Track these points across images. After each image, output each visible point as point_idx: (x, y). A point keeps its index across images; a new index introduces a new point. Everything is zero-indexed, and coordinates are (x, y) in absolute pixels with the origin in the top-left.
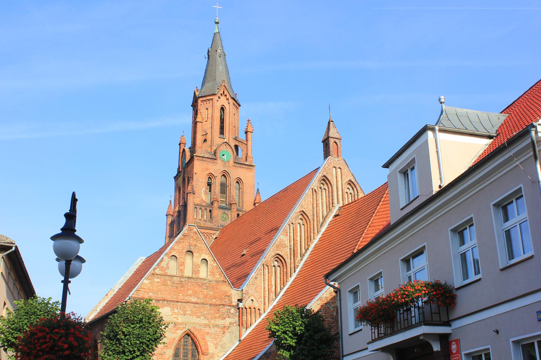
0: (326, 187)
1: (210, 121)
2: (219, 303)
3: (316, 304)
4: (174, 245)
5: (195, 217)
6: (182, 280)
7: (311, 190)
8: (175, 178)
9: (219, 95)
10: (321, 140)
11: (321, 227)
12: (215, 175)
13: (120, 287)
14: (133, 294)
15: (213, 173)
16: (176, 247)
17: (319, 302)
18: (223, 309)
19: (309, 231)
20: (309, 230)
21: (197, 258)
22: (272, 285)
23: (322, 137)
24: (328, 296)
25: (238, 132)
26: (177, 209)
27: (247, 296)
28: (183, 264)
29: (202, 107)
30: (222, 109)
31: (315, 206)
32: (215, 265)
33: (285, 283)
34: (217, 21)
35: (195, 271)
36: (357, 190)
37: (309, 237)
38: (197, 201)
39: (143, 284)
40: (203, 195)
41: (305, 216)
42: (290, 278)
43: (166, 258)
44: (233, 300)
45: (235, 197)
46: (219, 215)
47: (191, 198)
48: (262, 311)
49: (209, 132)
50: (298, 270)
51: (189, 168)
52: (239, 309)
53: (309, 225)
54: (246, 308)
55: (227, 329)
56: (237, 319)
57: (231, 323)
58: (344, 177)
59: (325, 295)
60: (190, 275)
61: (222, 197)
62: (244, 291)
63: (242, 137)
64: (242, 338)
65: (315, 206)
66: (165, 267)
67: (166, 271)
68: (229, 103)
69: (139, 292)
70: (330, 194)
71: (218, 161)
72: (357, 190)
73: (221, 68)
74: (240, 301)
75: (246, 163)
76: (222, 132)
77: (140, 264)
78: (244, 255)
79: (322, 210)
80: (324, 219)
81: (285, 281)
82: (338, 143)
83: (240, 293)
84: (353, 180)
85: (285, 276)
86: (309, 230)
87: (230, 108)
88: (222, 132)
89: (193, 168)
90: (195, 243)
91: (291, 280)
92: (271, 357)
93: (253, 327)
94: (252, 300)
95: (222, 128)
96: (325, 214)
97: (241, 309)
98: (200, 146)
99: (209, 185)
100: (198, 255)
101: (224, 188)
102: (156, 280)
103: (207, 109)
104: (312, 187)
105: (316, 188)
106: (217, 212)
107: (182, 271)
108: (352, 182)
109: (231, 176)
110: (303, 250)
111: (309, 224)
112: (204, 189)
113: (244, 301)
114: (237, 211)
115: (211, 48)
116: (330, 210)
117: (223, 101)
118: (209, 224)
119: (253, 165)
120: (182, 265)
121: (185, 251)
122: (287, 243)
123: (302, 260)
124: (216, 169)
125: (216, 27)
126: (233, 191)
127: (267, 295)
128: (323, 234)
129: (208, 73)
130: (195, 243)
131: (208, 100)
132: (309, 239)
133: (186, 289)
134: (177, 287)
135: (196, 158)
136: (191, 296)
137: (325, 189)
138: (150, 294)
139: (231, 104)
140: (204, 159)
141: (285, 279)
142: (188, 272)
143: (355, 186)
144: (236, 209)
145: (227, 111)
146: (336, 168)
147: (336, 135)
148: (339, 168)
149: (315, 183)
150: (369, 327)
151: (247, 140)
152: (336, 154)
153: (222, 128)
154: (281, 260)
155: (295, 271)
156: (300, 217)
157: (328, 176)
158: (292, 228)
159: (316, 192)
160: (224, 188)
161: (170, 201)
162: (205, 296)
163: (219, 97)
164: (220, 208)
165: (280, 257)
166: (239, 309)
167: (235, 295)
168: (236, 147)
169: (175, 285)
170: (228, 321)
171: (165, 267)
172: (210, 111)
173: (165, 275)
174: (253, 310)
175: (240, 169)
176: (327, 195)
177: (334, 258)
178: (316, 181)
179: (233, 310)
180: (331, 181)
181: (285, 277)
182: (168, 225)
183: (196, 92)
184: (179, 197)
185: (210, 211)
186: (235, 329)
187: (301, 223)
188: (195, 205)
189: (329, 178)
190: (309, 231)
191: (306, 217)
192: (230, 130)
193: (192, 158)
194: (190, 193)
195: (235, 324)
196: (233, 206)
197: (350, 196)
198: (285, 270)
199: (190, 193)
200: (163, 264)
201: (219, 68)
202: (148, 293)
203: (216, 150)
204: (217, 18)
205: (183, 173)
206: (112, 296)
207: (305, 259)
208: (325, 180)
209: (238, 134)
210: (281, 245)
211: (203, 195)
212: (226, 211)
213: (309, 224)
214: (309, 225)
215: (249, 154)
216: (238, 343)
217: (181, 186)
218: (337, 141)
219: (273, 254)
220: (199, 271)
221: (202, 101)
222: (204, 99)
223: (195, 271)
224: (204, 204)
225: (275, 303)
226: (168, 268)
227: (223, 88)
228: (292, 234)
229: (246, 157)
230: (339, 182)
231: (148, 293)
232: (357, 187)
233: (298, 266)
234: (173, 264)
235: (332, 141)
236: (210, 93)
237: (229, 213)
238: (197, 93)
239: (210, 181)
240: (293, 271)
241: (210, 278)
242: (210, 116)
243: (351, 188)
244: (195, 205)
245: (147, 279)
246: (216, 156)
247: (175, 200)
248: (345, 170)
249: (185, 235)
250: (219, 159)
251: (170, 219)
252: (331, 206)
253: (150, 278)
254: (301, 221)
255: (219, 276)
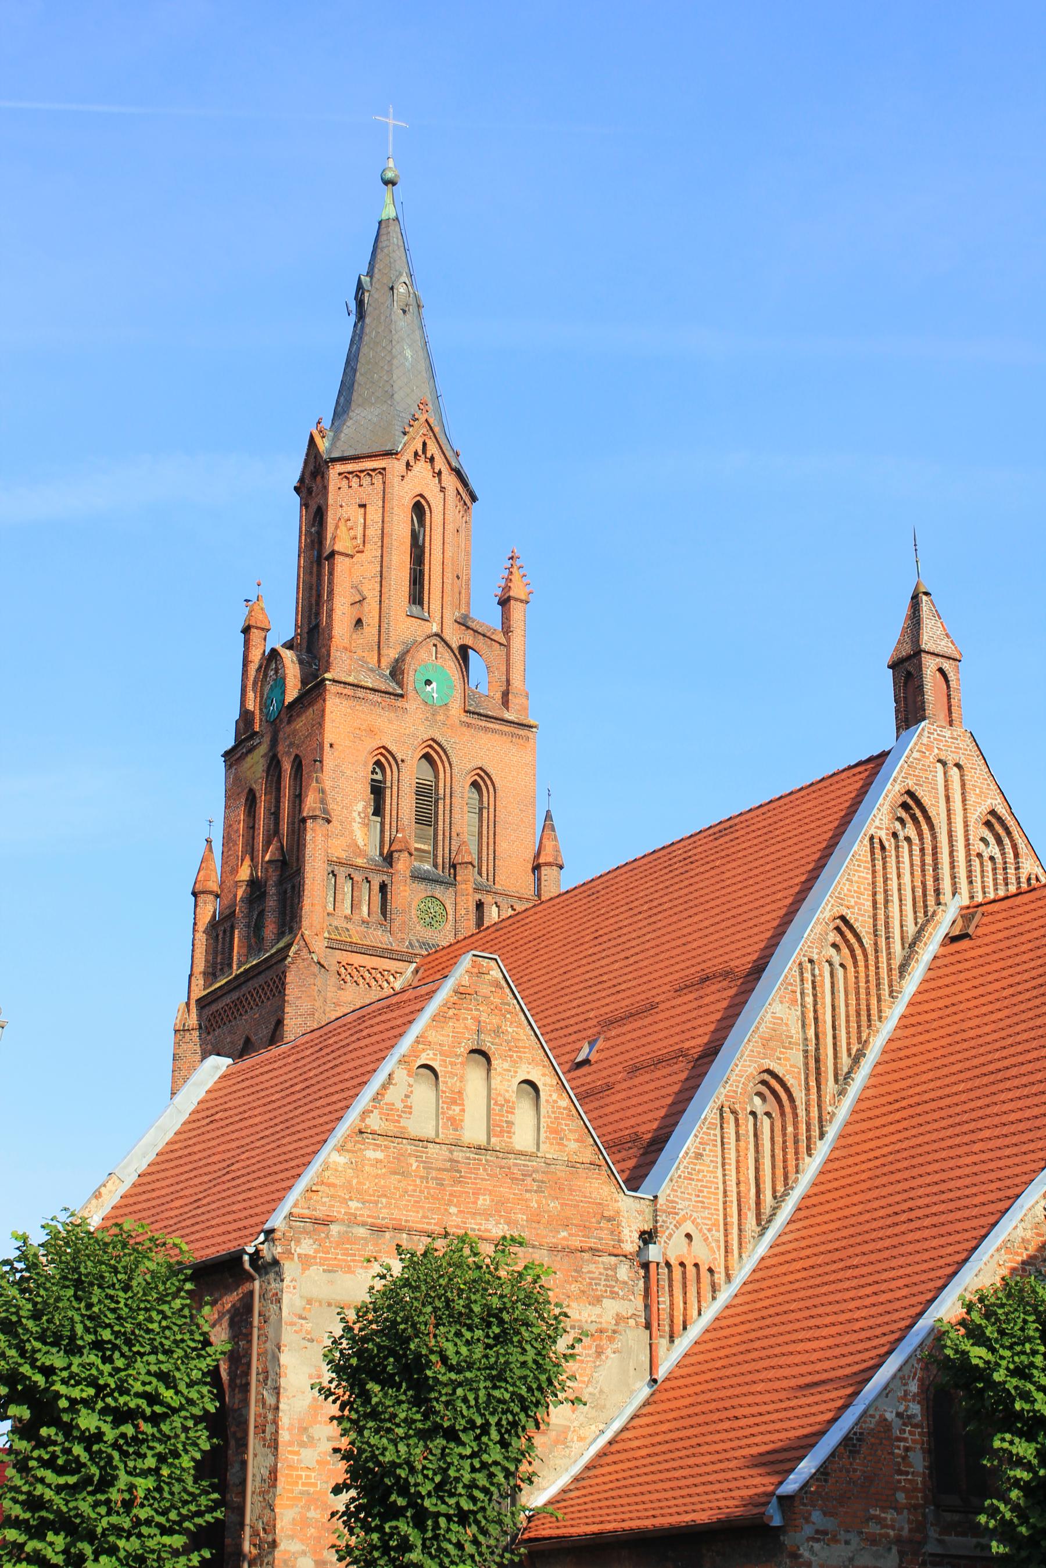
0: (911, 831)
1: (372, 551)
2: (578, 1245)
3: (993, 1263)
4: (428, 1027)
5: (330, 908)
6: (458, 1155)
7: (866, 842)
8: (227, 754)
9: (409, 456)
10: (887, 657)
11: (901, 976)
12: (399, 757)
13: (143, 1166)
14: (295, 1205)
15: (393, 748)
16: (432, 1036)
17: (1003, 1256)
18: (592, 1267)
19: (862, 991)
20: (862, 984)
21: (507, 1077)
22: (748, 1183)
23: (888, 643)
24: (1029, 1234)
25: (468, 595)
26: (244, 873)
27: (671, 1222)
28: (457, 1098)
29: (342, 497)
30: (419, 509)
31: (880, 898)
32: (564, 1103)
33: (792, 1176)
34: (389, 175)
35: (497, 1122)
36: (1015, 847)
37: (864, 1013)
38: (339, 852)
39: (326, 1167)
40: (356, 826)
41: (849, 936)
42: (807, 1159)
43: (401, 1075)
44: (626, 1231)
45: (466, 837)
46: (414, 905)
47: (320, 839)
48: (720, 1277)
49: (371, 591)
50: (832, 1131)
51: (300, 724)
52: (646, 1266)
53: (862, 969)
54: (668, 1265)
55: (611, 1339)
56: (640, 1303)
57: (619, 1319)
58: (971, 799)
59: (1020, 1232)
60: (482, 1140)
61: (420, 838)
62: (661, 1201)
63: (488, 616)
64: (661, 1373)
65: (880, 898)
66: (399, 1105)
67: (403, 1122)
68: (443, 489)
69: (314, 1196)
70: (929, 859)
71: (412, 704)
72: (1015, 847)
73: (408, 353)
74: (647, 1237)
75: (507, 716)
76: (417, 596)
77: (209, 1085)
78: (586, 1062)
79: (902, 917)
80: (912, 946)
81: (791, 1169)
82: (951, 676)
83: (648, 1212)
84: (1001, 811)
85: (791, 1150)
86: (862, 984)
87: (443, 508)
88: (417, 596)
89: (321, 725)
90: (495, 1020)
91: (812, 1167)
92: (863, 1450)
93: (695, 1331)
94: (688, 1236)
95: (417, 580)
96: (911, 929)
97: (653, 1267)
98: (345, 642)
99: (378, 791)
100: (506, 1065)
101: (428, 800)
102: (371, 1154)
103: (363, 506)
104: (872, 831)
105: (883, 834)
106: (407, 895)
107: (456, 1123)
108: (999, 819)
109: (453, 760)
110: (845, 1061)
111: (861, 963)
112: (360, 806)
113: (662, 1238)
114: (477, 890)
115: (370, 273)
116: (929, 918)
117: (422, 479)
118: (378, 937)
119: (532, 722)
120: (454, 1102)
121: (462, 1050)
122: (795, 1030)
123: (842, 1093)
124: (404, 731)
125: (388, 199)
126: (462, 817)
127: (735, 1219)
128: (910, 1004)
129: (361, 368)
130: (495, 1020)
131: (369, 472)
132: (865, 1018)
133: (469, 1189)
134: (440, 1184)
135: (331, 688)
136: (486, 1215)
137: (908, 839)
138: (354, 1205)
139: (451, 492)
140: (360, 693)
141: (791, 1163)
142: (474, 1131)
143: (1009, 833)
144: (471, 886)
145: (435, 517)
146: (944, 764)
147: (943, 646)
148: (958, 766)
149: (879, 816)
150: (363, 1297)
151: (507, 630)
152: (943, 714)
153: (417, 580)
154: (774, 1092)
155: (822, 1136)
156: (833, 937)
157: (920, 793)
158: (808, 975)
159: (883, 848)
160: (428, 800)
161: (209, 841)
162: (535, 1219)
163: (408, 464)
164: (419, 877)
165: (774, 1083)
166: (646, 1266)
167: (631, 1212)
168: (464, 650)
169: (434, 1174)
170: (611, 1308)
171: (399, 1105)
172: (374, 513)
173: (400, 1137)
174: (691, 1270)
175: (485, 738)
176: (917, 860)
177: (1003, 1097)
178: (886, 806)
179: (624, 1272)
180: (932, 813)
181: (791, 1156)
182: (202, 926)
183: (318, 440)
184: (252, 828)
185: (383, 887)
186: (635, 1337)
187: (836, 960)
188: (330, 862)
189: (926, 801)
190: (862, 991)
191: (853, 940)
192: (448, 587)
193: (314, 689)
194: (314, 818)
195: (632, 1322)
196: (462, 873)
197: (989, 866)
198: (790, 1129)
199: (314, 818)
200: (393, 1096)
201: (402, 353)
202: (344, 1202)
203: (397, 661)
204: (391, 163)
205: (266, 740)
206: (115, 1200)
207: (854, 1089)
208: (912, 806)
209: (468, 604)
210: (773, 1041)
211: (356, 826)
212: (438, 891)
213: (861, 963)
214: (862, 969)
215: (516, 682)
216: (646, 1392)
217: (260, 789)
218: (946, 665)
219: (752, 1069)
220: (510, 1124)
221: (345, 476)
222: (350, 467)
223: (497, 1122)
224: (360, 861)
225: (762, 1248)
226: (408, 1109)
227: (424, 430)
228: (809, 999)
229: (506, 694)
230: (959, 820)
231: (344, 1202)
232: (1016, 835)
233: (833, 1115)
234: (423, 1094)
235: (930, 665)
236: (376, 448)
237: (446, 896)
238: (323, 445)
239: (379, 777)
240: (816, 1133)
241: (548, 1150)
242: (374, 532)
243: (991, 840)
244: (330, 862)
245: (341, 1149)
246: (401, 684)
247: (228, 840)
248: (976, 774)
249: (460, 993)
250: (411, 694)
251: (209, 909)
252: (931, 900)
253: (349, 1146)
254: (832, 951)
255: (576, 1145)
